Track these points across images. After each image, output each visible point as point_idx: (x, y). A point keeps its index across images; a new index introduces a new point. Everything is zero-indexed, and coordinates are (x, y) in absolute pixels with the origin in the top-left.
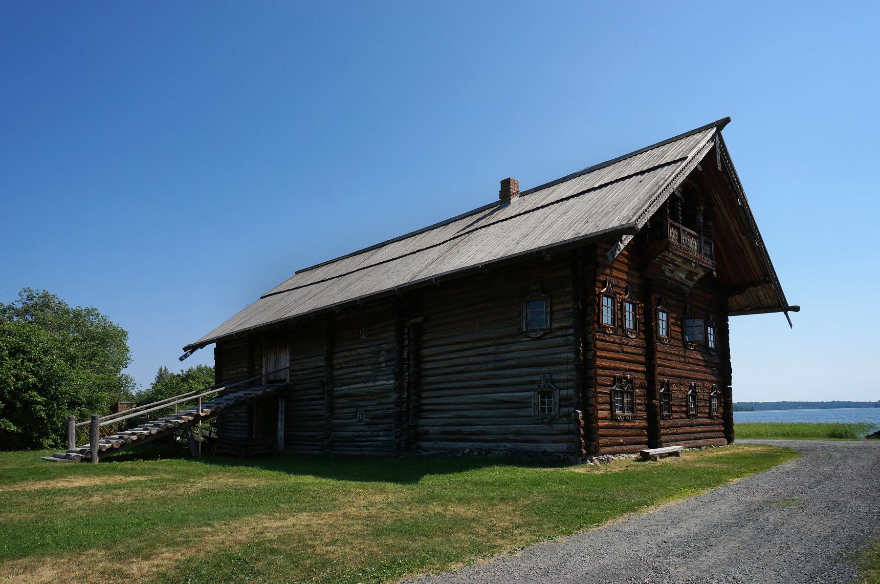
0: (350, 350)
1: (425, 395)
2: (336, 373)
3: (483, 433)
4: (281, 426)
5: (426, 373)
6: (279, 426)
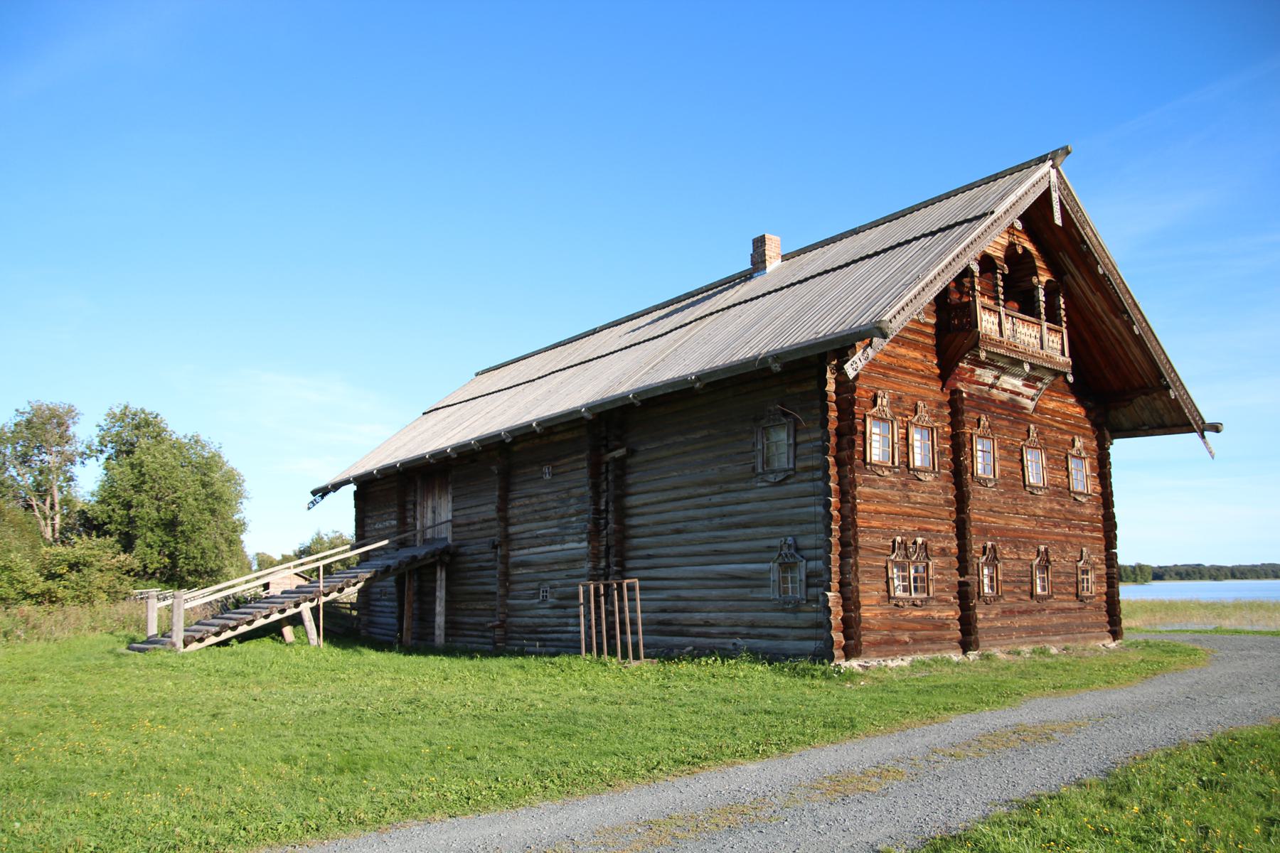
4: (440, 608)
5: (640, 531)
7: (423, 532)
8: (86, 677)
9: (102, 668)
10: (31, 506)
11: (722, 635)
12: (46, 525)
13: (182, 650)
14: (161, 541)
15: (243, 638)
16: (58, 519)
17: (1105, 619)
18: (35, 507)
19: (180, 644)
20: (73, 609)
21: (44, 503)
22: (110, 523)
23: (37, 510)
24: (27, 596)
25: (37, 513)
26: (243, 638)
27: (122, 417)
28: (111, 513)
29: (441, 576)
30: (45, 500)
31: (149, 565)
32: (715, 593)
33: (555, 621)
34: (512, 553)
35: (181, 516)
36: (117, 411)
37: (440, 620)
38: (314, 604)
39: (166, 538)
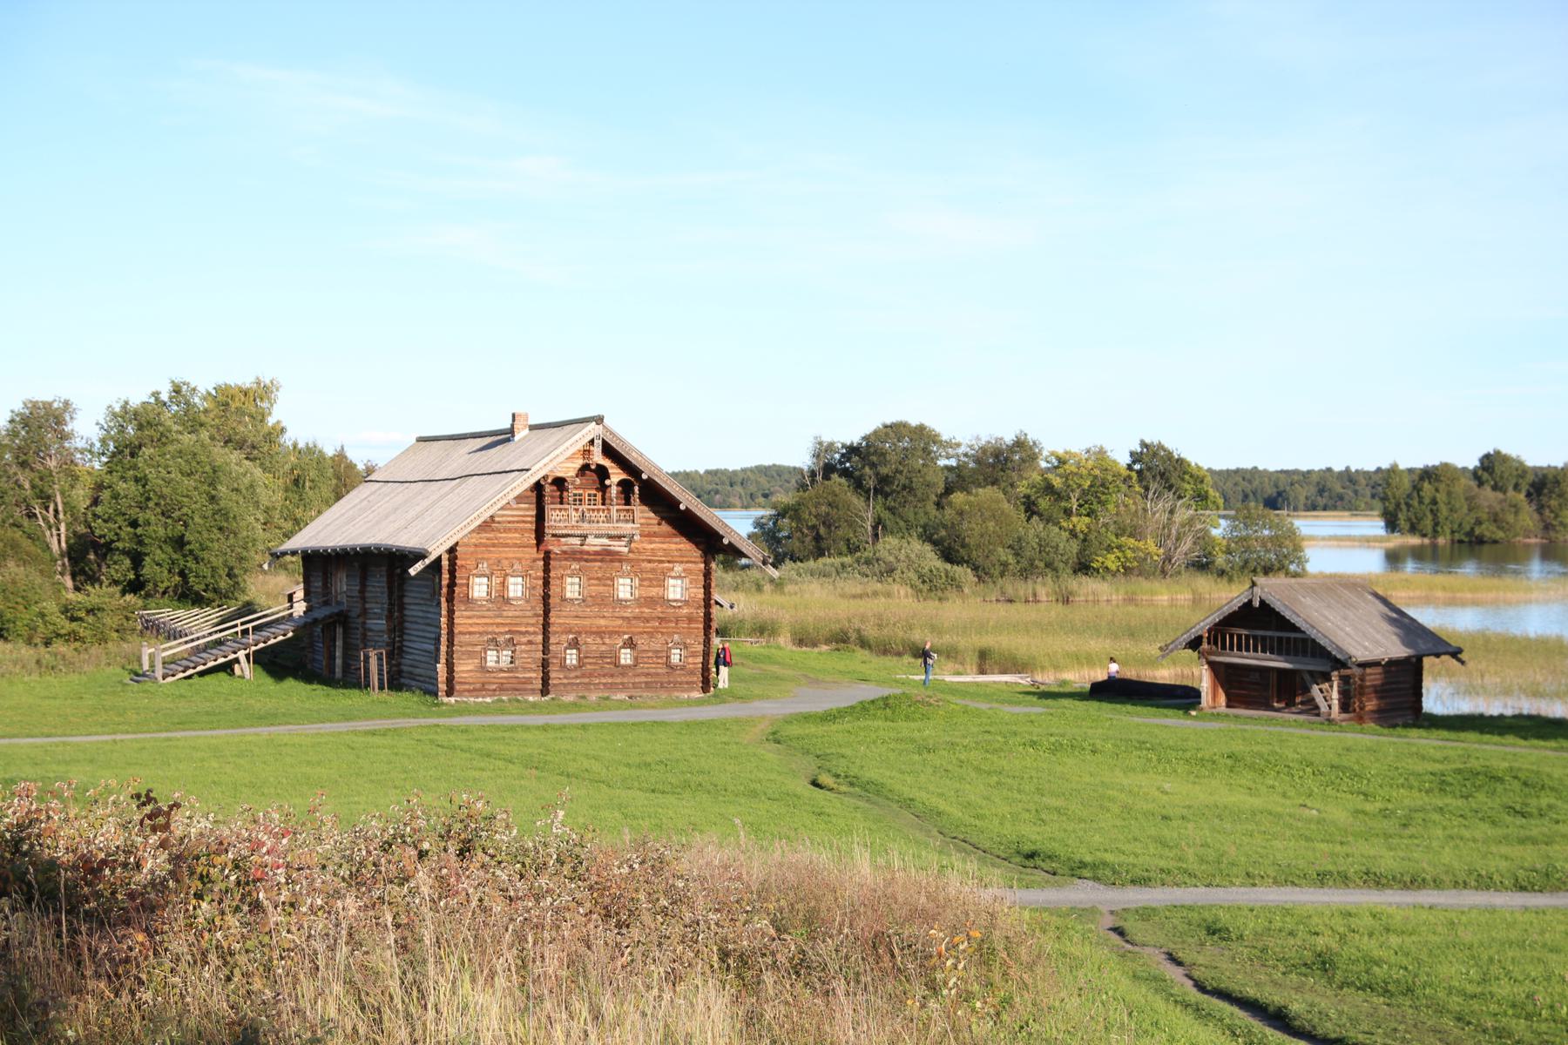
4: (338, 653)
5: (410, 619)
6: (337, 654)
7: (336, 597)
8: (106, 697)
9: (114, 693)
10: (35, 515)
12: (52, 535)
13: (162, 681)
14: (170, 558)
15: (202, 674)
16: (63, 528)
18: (39, 515)
19: (160, 678)
20: (95, 650)
21: (47, 509)
22: (118, 540)
23: (41, 519)
24: (58, 635)
25: (41, 523)
26: (202, 674)
28: (118, 531)
29: (339, 631)
30: (49, 507)
31: (159, 584)
34: (368, 621)
35: (188, 537)
36: (117, 409)
37: (339, 662)
38: (247, 651)
39: (175, 556)
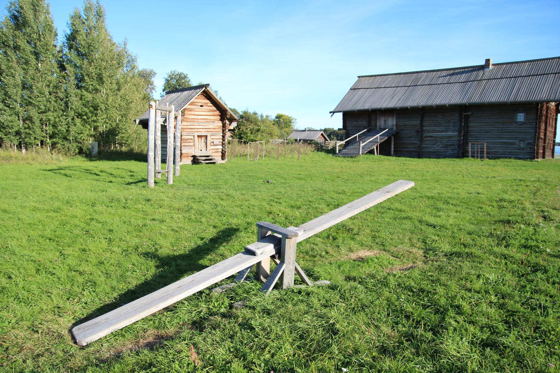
0: (433, 121)
1: (469, 138)
2: (424, 128)
3: (496, 152)
4: (393, 146)
5: (471, 131)
11: (501, 154)
17: (551, 153)
27: (171, 77)
32: (498, 146)
33: (443, 150)
37: (393, 150)
